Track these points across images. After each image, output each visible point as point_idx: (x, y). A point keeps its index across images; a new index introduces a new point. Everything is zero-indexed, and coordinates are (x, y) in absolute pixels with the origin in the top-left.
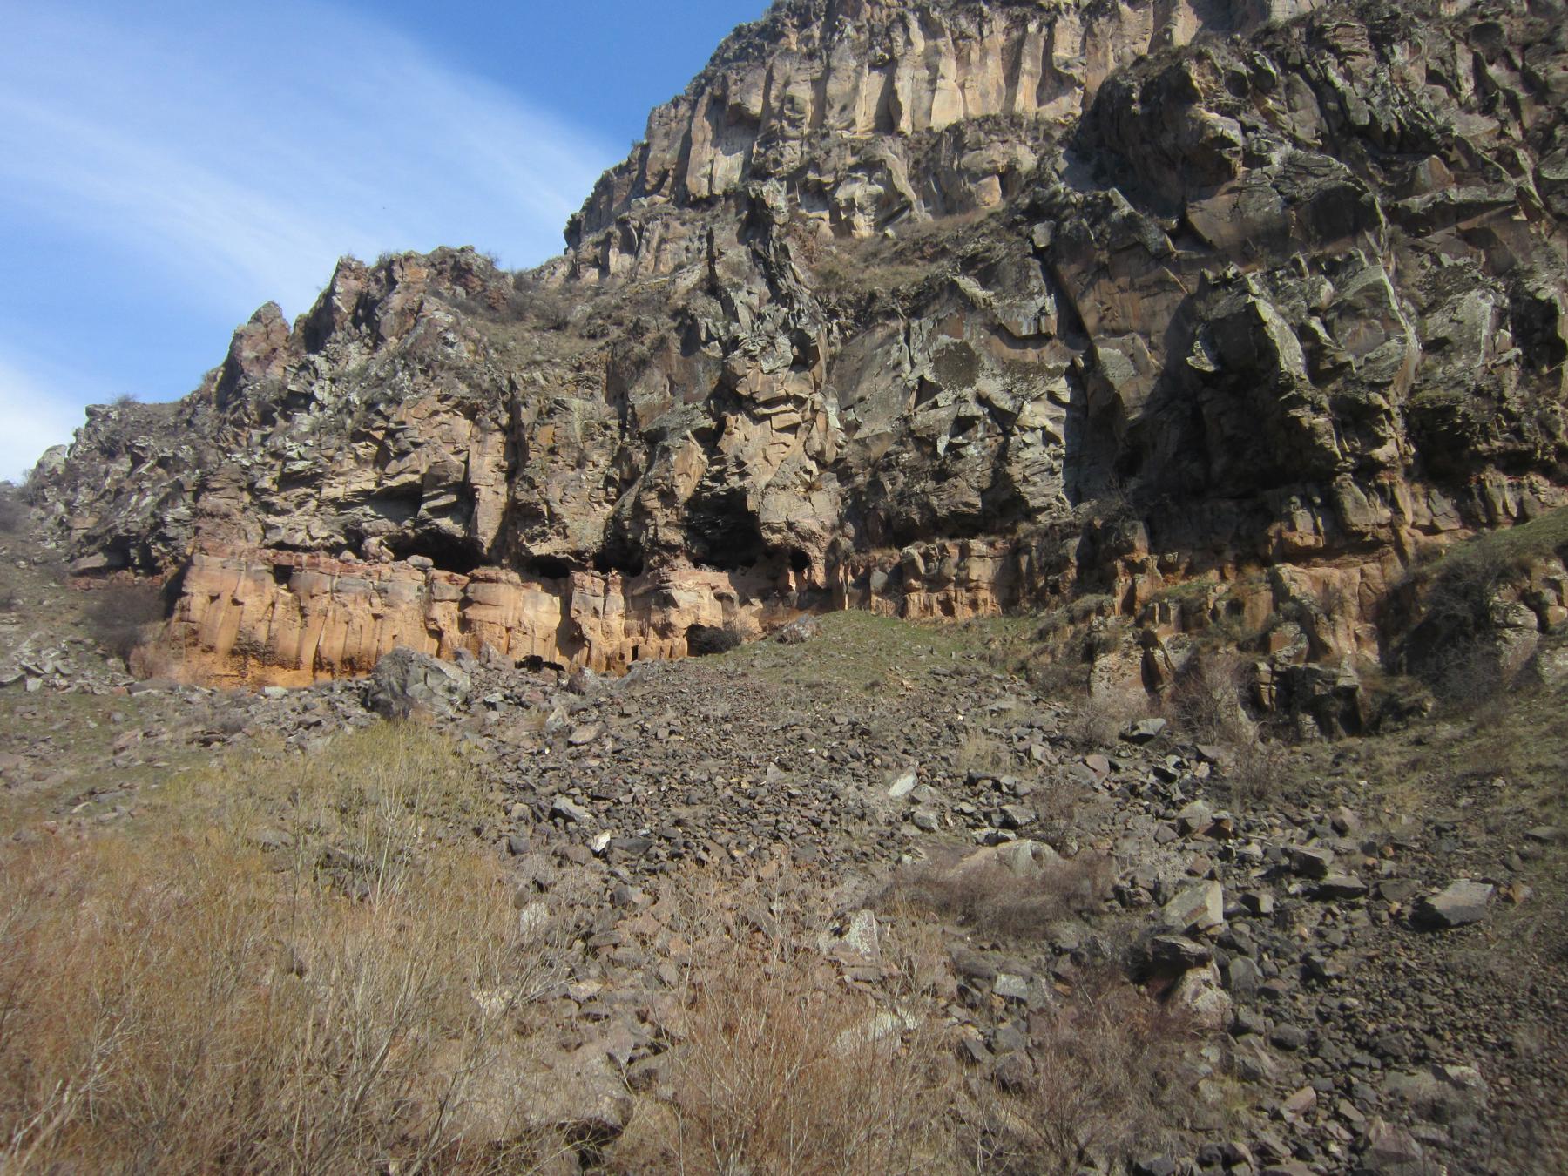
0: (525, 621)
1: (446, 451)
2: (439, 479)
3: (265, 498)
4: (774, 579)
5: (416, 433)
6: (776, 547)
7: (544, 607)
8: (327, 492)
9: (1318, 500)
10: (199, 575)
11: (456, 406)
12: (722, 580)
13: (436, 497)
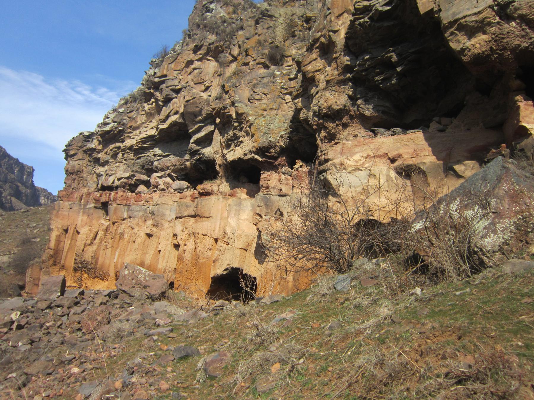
0: (229, 231)
1: (198, 90)
2: (195, 115)
3: (95, 155)
4: (499, 127)
5: (176, 82)
6: (479, 60)
8: (129, 142)
9: (159, 344)
10: (57, 216)
11: (207, 54)
12: (413, 145)
13: (199, 130)
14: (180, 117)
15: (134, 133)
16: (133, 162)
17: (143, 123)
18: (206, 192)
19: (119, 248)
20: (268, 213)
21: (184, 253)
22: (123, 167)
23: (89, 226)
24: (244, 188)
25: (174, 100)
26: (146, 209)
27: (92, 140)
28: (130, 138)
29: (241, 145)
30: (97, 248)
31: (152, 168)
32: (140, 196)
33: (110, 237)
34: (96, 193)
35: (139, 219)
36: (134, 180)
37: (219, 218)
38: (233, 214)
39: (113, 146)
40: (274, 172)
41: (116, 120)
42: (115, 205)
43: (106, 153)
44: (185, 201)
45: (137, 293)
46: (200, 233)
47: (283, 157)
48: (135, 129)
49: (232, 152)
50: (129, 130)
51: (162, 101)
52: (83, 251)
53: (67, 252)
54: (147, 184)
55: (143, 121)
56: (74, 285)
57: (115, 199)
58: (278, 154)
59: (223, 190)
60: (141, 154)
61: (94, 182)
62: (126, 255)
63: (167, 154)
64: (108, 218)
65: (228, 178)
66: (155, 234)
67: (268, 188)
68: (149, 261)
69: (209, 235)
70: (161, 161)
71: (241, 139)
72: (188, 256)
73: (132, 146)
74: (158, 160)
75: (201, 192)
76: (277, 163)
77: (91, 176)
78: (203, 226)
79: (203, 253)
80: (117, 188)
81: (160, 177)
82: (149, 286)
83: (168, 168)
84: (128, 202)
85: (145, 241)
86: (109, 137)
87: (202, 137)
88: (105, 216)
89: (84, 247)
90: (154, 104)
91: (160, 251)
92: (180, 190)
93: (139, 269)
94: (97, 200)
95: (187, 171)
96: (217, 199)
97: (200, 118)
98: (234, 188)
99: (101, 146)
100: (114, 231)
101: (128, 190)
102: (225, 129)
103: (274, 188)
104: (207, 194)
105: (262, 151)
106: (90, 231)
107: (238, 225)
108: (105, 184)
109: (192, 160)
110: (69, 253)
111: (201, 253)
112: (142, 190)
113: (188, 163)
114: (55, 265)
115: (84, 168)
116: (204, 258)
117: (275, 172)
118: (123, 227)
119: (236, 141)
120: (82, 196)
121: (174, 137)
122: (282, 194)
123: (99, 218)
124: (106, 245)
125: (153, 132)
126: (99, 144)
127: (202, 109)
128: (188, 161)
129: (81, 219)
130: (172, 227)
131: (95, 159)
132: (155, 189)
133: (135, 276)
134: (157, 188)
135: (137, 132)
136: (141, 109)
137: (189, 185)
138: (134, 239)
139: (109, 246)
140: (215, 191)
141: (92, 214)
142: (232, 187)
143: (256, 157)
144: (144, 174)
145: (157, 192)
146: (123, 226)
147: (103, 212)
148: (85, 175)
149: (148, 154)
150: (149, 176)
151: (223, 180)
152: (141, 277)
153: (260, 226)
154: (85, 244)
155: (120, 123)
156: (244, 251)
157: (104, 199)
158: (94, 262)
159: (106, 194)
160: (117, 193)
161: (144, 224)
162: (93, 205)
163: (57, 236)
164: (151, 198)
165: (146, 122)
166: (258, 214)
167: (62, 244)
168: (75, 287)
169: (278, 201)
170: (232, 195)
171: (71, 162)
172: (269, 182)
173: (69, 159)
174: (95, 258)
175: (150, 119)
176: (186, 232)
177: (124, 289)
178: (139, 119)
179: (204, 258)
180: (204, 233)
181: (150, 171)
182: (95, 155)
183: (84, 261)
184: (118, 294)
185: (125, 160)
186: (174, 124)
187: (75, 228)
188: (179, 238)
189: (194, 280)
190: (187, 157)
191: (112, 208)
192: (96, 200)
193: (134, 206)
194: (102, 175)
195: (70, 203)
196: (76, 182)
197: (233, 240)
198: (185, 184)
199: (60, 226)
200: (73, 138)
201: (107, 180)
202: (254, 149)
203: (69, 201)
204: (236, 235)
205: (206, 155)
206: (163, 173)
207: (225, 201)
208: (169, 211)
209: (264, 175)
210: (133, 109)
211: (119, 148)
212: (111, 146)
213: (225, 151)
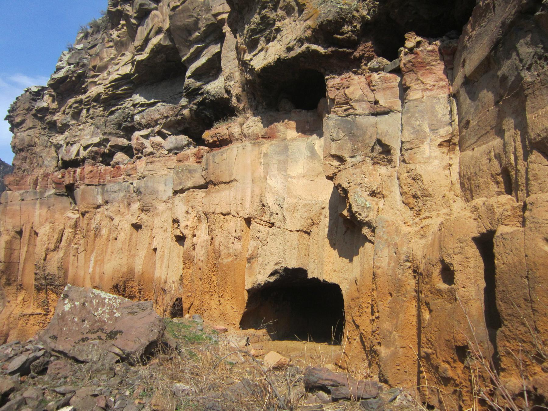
0: (270, 201)
2: (189, 30)
3: (48, 118)
7: (299, 167)
8: (93, 91)
13: (196, 56)
14: (165, 37)
15: (101, 76)
16: (103, 120)
17: (112, 59)
18: (220, 141)
19: (95, 251)
20: (357, 150)
21: (194, 249)
22: (89, 129)
23: (51, 223)
24: (290, 120)
25: (154, 12)
26: (128, 187)
27: (43, 97)
28: (96, 85)
29: (279, 37)
30: (65, 254)
31: (133, 126)
32: (119, 168)
33: (80, 236)
34: (56, 173)
35: (119, 203)
36: (108, 147)
37: (249, 180)
38: (274, 169)
39: (73, 100)
40: (351, 73)
41: (72, 61)
42: (82, 187)
43: (64, 113)
44: (187, 163)
45: (92, 352)
46: (218, 211)
47: (367, 42)
48: (102, 69)
49: (263, 53)
50: (92, 73)
51: (135, 18)
52: (45, 260)
53: (24, 263)
54: (128, 150)
55: (112, 56)
56: (39, 311)
57: (82, 179)
58: (357, 36)
59: (250, 131)
60: (114, 105)
61: (53, 157)
62: (105, 260)
63: (152, 101)
64: (77, 208)
65: (256, 109)
66: (145, 224)
67: (347, 103)
68: (140, 267)
69: (234, 213)
70: (144, 113)
71: (278, 24)
72: (200, 254)
73: (99, 95)
74: (140, 112)
75: (211, 141)
76: (357, 54)
77: (47, 149)
78: (220, 199)
79: (227, 247)
80: (84, 160)
81: (146, 137)
82: (121, 332)
83: (156, 122)
84: (102, 180)
85: (131, 236)
86: (66, 87)
87: (203, 65)
88: (73, 205)
89: (46, 255)
90: (125, 28)
91: (155, 250)
92: (176, 150)
93: (96, 296)
94: (58, 184)
95: (187, 125)
96: (241, 148)
97: (197, 34)
98: (272, 123)
99: (56, 103)
100: (85, 226)
101: (101, 162)
102: (243, 18)
103: (360, 100)
104: (222, 143)
105: (325, 32)
106: (53, 229)
107: (288, 189)
108: (67, 158)
109: (191, 105)
110: (27, 265)
111: (222, 247)
112: (120, 160)
113: (186, 112)
114: (9, 285)
115: (37, 139)
116: (229, 255)
117: (355, 73)
118: (98, 218)
119: (267, 32)
120: (37, 179)
121: (161, 72)
122: (378, 110)
123: (65, 209)
124: (77, 249)
125: (128, 69)
126: (53, 101)
127: (198, 19)
128: (185, 107)
129: (38, 213)
130: (171, 209)
131: (49, 123)
132: (140, 155)
133: (89, 312)
134: (142, 153)
135: (104, 74)
136: (107, 39)
137: (191, 140)
138: (115, 235)
139: (81, 249)
140: (236, 135)
141: (54, 205)
142: (267, 123)
143: (314, 47)
144: (122, 137)
145: (143, 158)
146: (98, 217)
147: (70, 200)
148: (38, 150)
149: (124, 106)
150: (130, 139)
151: (248, 115)
152: (102, 313)
153: (343, 180)
154: (47, 250)
155: (78, 63)
156: (306, 235)
157: (68, 180)
158: (62, 275)
159: (69, 173)
160: (84, 169)
161: (128, 209)
162: (53, 191)
163: (6, 243)
164: (134, 169)
165: (116, 58)
166: (334, 156)
167: (16, 253)
168: (40, 314)
169: (375, 125)
170: (267, 137)
171: (19, 134)
172: (347, 91)
173: (15, 130)
174: (63, 268)
175: (121, 51)
176: (193, 215)
177: (61, 348)
178: (105, 55)
179: (229, 255)
180: (224, 211)
181: (129, 132)
182: (48, 118)
183: (48, 275)
184: (48, 363)
185: (91, 118)
186: (158, 50)
187: (32, 228)
188: (182, 225)
189: (216, 295)
190: (184, 101)
191: (78, 193)
192: (56, 184)
193: (111, 185)
194: (61, 146)
195: (21, 192)
196: (28, 160)
197: (280, 217)
198: (183, 139)
199: (10, 227)
200: (17, 98)
201: (68, 152)
202: (309, 33)
203: (19, 189)
204: (285, 206)
205: (213, 93)
206: (150, 130)
207: (257, 149)
208: (164, 185)
209: (333, 81)
210: (96, 42)
211: (80, 102)
212: (70, 100)
213: (247, 57)
